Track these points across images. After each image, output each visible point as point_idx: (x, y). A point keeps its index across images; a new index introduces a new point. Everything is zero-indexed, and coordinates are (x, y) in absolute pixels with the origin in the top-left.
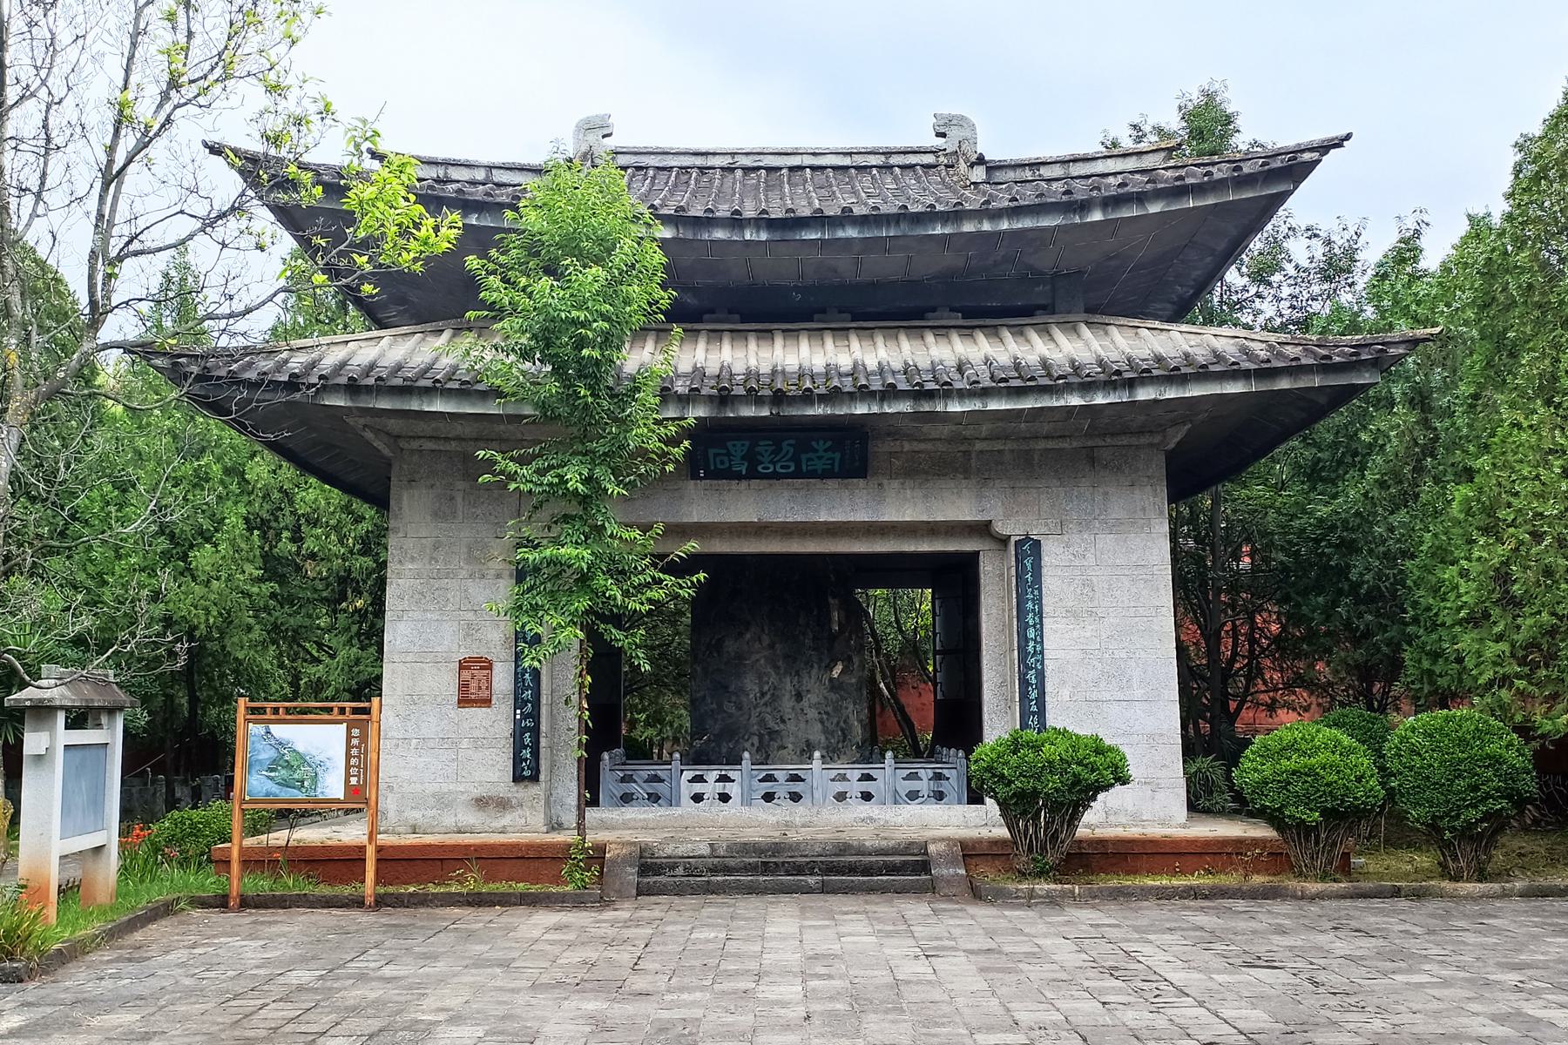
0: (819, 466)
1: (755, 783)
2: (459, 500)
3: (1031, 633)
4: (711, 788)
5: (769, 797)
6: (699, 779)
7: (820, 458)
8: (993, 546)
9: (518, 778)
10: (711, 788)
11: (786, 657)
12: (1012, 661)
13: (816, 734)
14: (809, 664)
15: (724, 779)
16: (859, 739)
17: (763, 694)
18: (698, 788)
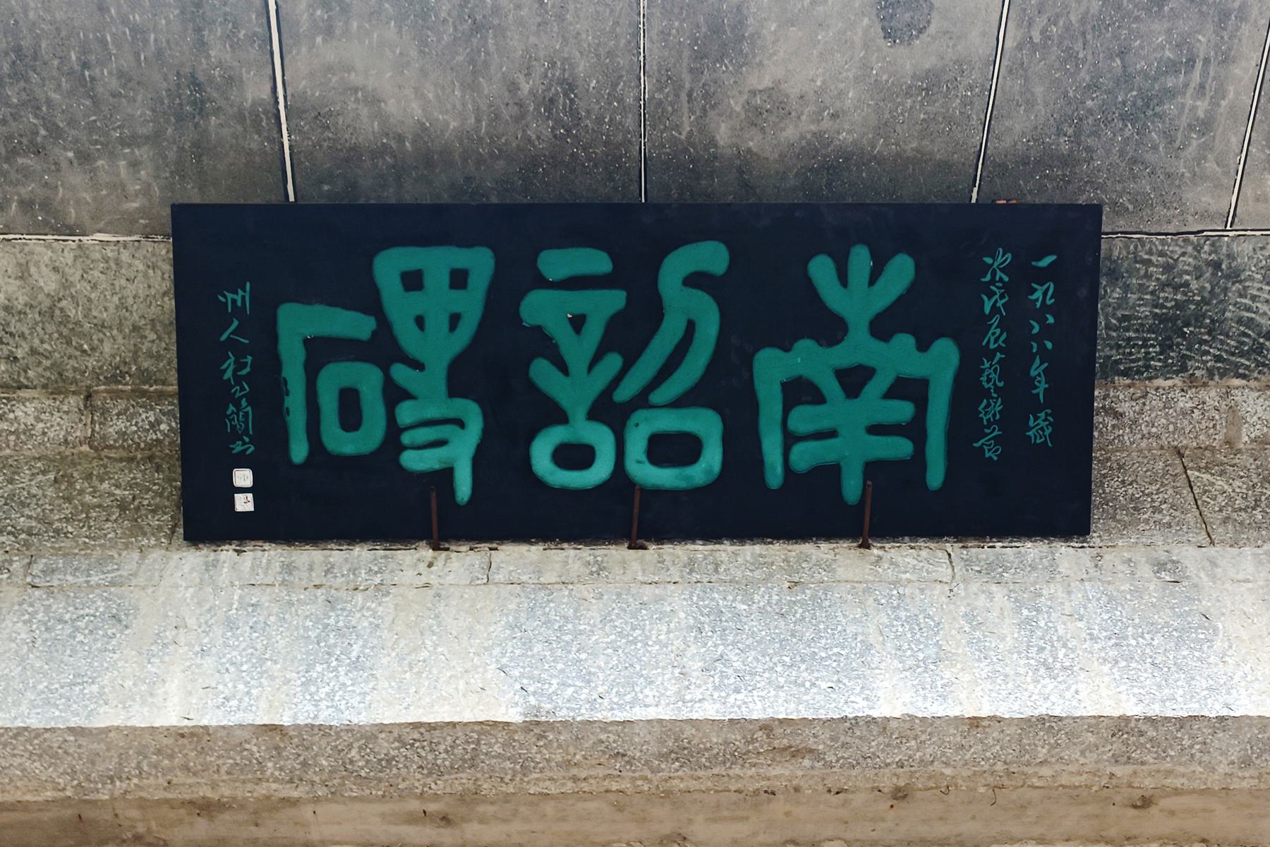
0: (850, 439)
7: (854, 380)
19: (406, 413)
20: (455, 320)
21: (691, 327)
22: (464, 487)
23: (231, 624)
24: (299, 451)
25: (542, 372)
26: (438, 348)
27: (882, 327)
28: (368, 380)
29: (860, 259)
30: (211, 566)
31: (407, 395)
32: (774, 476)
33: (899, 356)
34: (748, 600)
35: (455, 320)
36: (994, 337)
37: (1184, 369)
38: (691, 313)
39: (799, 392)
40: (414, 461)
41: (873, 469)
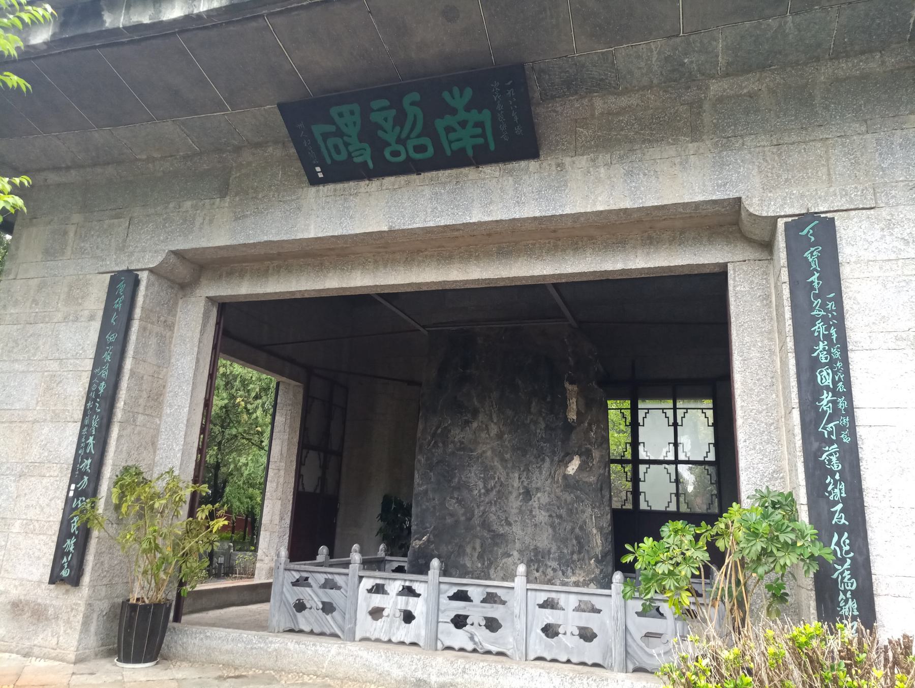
0: (467, 140)
1: (444, 600)
2: (71, 234)
3: (825, 377)
4: (392, 602)
5: (460, 622)
6: (378, 589)
7: (463, 124)
8: (750, 253)
9: (55, 579)
10: (392, 602)
11: (515, 449)
12: (790, 432)
13: (544, 540)
14: (540, 457)
15: (409, 592)
16: (598, 550)
17: (488, 491)
18: (377, 600)
19: (351, 148)
20: (355, 123)
21: (415, 116)
22: (371, 165)
23: (323, 208)
24: (329, 161)
25: (380, 133)
26: (353, 132)
27: (468, 109)
28: (339, 141)
29: (456, 90)
30: (318, 191)
31: (350, 144)
32: (449, 153)
33: (474, 116)
34: (444, 189)
35: (355, 123)
36: (499, 107)
37: (576, 93)
38: (415, 112)
39: (449, 130)
40: (358, 160)
41: (474, 147)
